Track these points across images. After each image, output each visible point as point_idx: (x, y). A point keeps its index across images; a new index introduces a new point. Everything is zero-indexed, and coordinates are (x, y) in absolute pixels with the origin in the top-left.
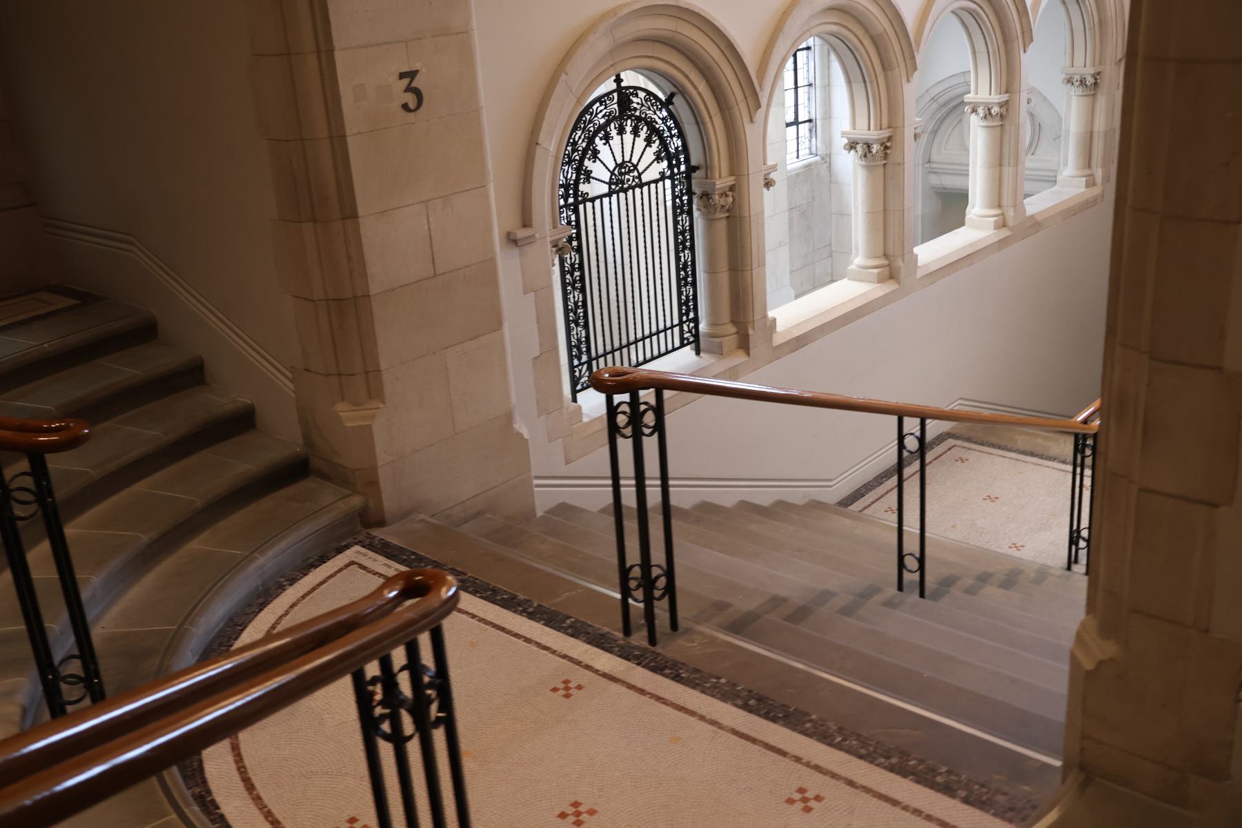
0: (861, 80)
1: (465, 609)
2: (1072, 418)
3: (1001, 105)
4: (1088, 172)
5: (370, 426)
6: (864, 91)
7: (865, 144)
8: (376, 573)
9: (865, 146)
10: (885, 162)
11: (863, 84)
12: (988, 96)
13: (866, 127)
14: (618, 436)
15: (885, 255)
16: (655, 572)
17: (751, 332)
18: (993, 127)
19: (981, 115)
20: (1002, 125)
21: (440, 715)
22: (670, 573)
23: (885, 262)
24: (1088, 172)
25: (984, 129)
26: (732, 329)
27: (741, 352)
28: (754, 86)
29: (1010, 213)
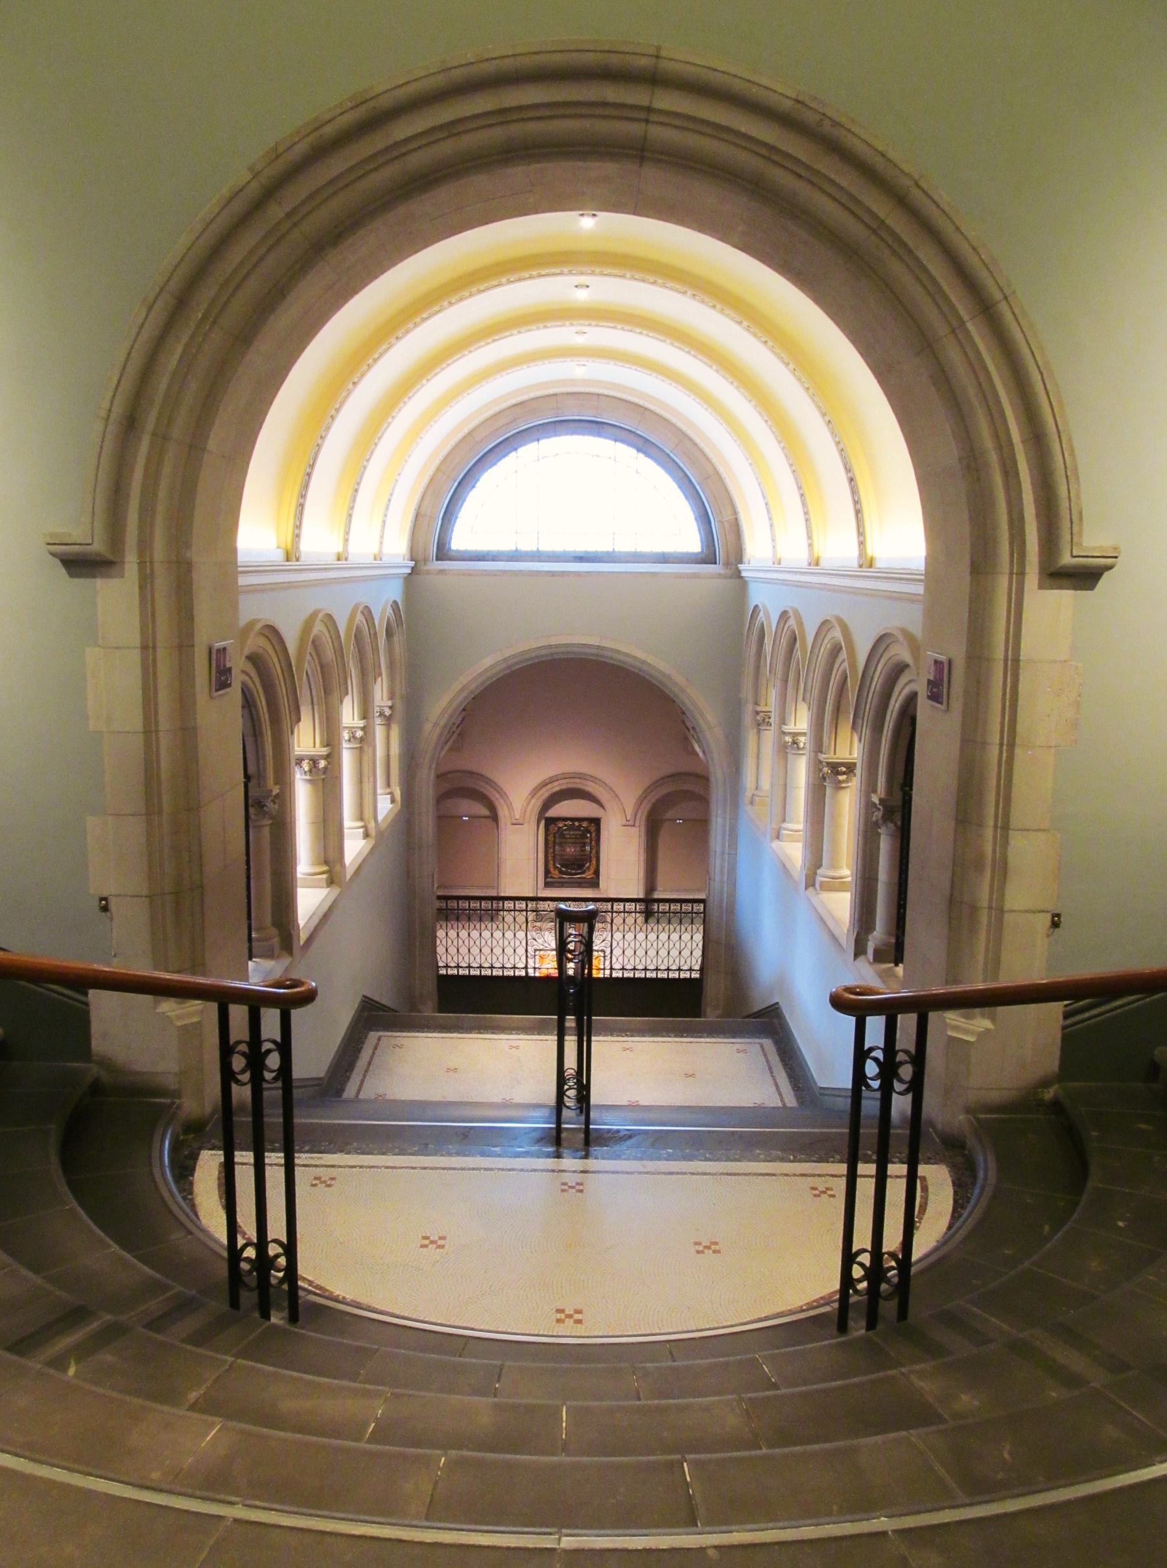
0: (310, 702)
1: (864, 1173)
2: (68, 1165)
3: (363, 729)
4: (389, 790)
5: (596, 822)
6: (311, 712)
7: (310, 760)
8: (780, 1094)
9: (311, 762)
10: (324, 777)
11: (310, 706)
12: (352, 722)
13: (312, 745)
14: (279, 1039)
15: (326, 862)
16: (274, 1249)
17: (292, 932)
18: (354, 748)
19: (306, 769)
20: (360, 747)
21: (699, 1524)
22: (290, 1249)
23: (325, 868)
24: (389, 790)
25: (350, 750)
26: (274, 931)
27: (285, 953)
28: (672, 424)
29: (372, 825)
